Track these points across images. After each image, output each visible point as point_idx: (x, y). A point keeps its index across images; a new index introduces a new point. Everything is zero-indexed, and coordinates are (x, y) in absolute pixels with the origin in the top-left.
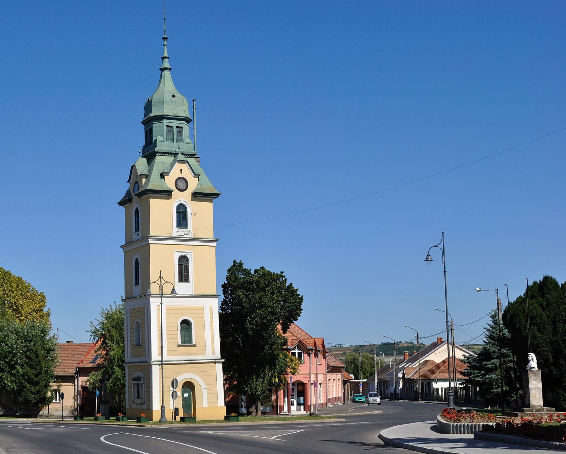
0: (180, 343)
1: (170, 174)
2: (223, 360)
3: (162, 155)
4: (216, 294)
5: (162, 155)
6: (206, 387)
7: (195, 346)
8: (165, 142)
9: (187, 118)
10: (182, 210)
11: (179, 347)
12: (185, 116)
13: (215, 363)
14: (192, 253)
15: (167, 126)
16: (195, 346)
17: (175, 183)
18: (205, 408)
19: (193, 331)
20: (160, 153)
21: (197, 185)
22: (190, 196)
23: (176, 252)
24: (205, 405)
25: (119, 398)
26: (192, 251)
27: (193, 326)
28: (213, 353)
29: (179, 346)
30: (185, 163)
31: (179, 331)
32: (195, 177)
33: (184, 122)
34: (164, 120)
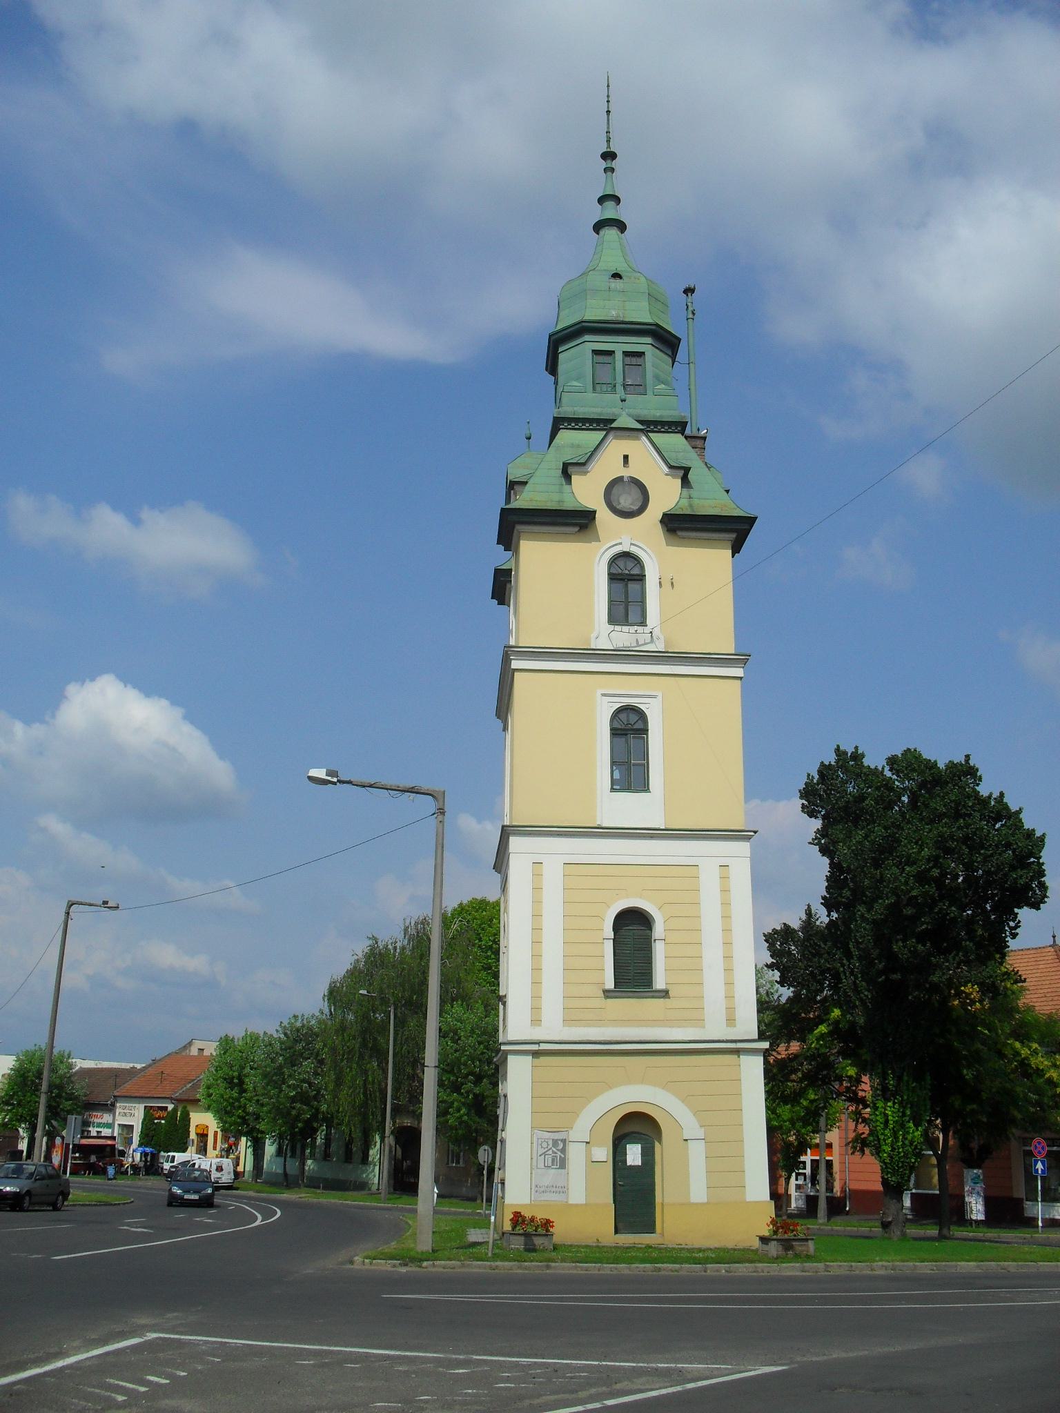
0: (610, 984)
1: (590, 467)
2: (766, 1045)
6: (700, 1133)
7: (665, 994)
8: (590, 395)
9: (657, 325)
10: (626, 567)
12: (650, 320)
13: (737, 1052)
14: (660, 698)
16: (665, 994)
19: (659, 951)
20: (570, 420)
23: (604, 695)
24: (698, 1192)
26: (660, 695)
27: (659, 930)
28: (731, 1021)
29: (607, 994)
31: (609, 948)
33: (649, 340)
34: (587, 337)
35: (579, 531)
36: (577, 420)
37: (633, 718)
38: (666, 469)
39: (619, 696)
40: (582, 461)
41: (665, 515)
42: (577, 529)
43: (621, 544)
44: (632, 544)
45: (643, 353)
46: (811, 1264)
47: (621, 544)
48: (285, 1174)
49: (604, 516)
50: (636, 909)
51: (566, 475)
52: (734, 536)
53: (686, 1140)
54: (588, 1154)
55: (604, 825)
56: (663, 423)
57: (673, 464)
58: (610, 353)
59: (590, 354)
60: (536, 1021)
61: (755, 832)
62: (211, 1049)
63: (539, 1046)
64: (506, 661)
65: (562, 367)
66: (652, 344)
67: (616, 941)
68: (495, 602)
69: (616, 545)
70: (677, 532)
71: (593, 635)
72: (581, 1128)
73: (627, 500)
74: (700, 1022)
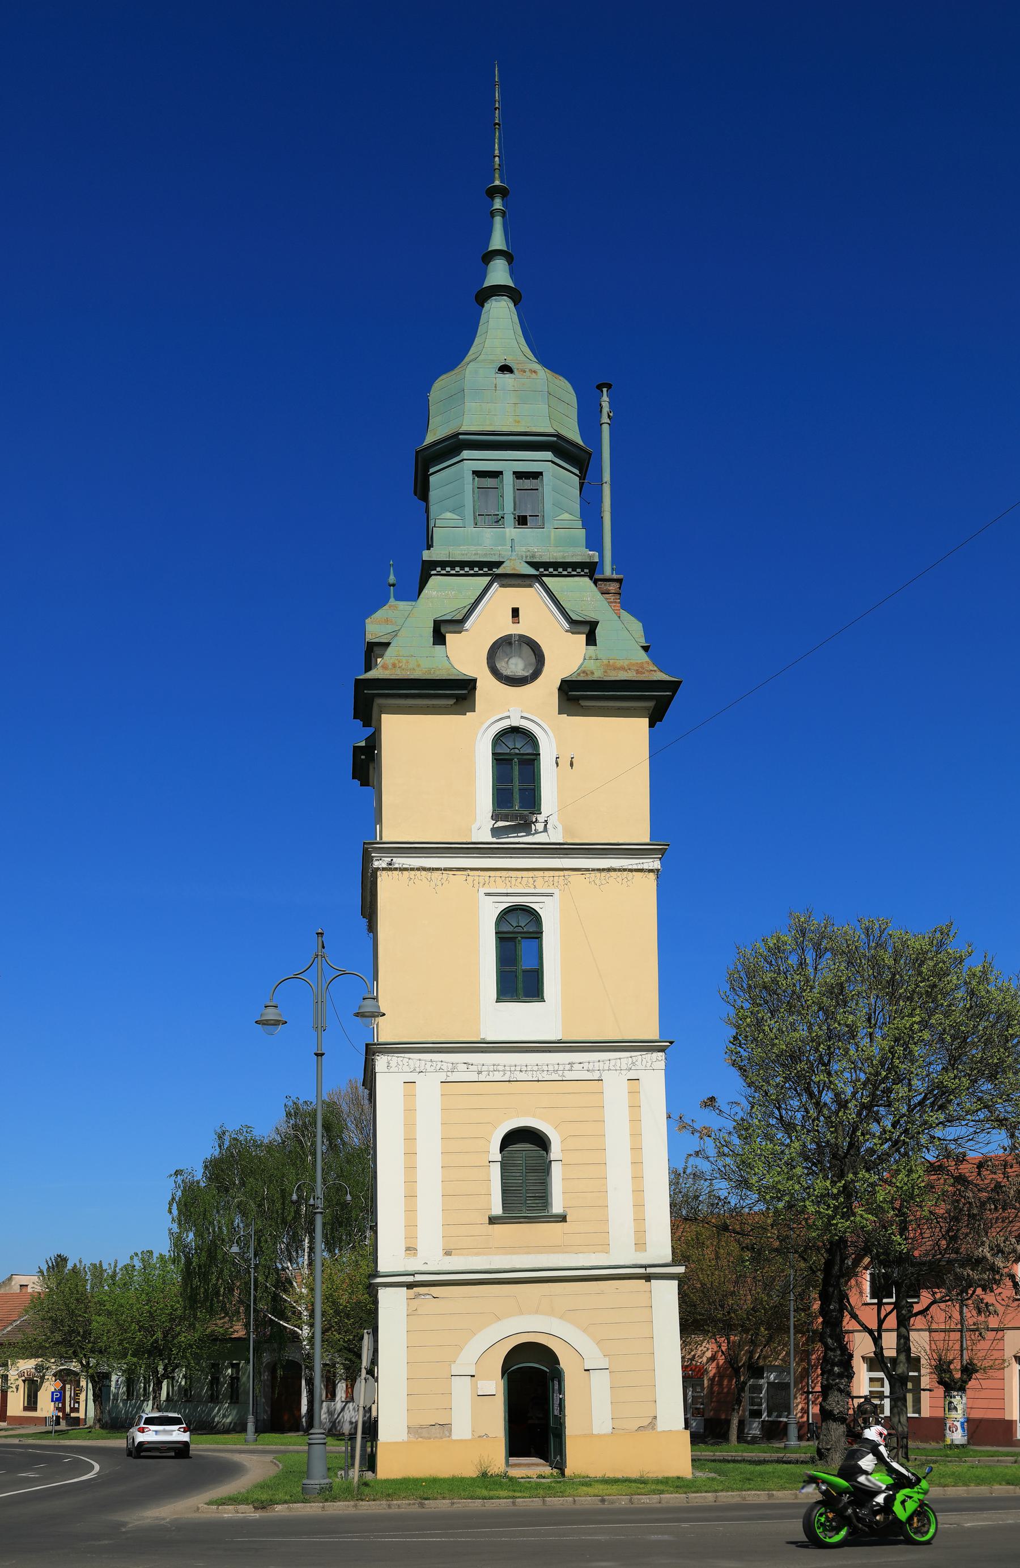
1: (467, 625)
2: (681, 1269)
4: (657, 1038)
5: (555, 573)
7: (563, 1218)
8: (471, 530)
9: (558, 436)
10: (519, 745)
11: (494, 1223)
12: (550, 430)
13: (648, 1278)
15: (478, 474)
16: (563, 1218)
17: (543, 664)
18: (599, 1436)
19: (556, 1170)
20: (443, 564)
21: (582, 660)
22: (554, 699)
23: (488, 894)
27: (556, 1151)
28: (640, 1245)
29: (493, 1220)
30: (531, 586)
31: (496, 1171)
32: (573, 633)
33: (549, 455)
34: (466, 454)
36: (453, 564)
37: (523, 920)
38: (566, 626)
39: (507, 895)
40: (459, 617)
41: (564, 682)
42: (451, 702)
43: (509, 717)
44: (522, 717)
45: (541, 473)
46: (725, 1493)
47: (509, 717)
49: (487, 685)
50: (528, 1129)
51: (439, 639)
52: (651, 704)
53: (588, 1370)
54: (474, 1387)
55: (489, 1039)
56: (565, 565)
57: (574, 617)
58: (497, 474)
59: (469, 476)
60: (411, 1250)
61: (671, 1043)
62: (34, 1284)
64: (367, 859)
65: (433, 494)
66: (553, 462)
67: (504, 1166)
68: (357, 782)
69: (501, 719)
70: (580, 702)
71: (474, 827)
72: (467, 1360)
73: (516, 666)
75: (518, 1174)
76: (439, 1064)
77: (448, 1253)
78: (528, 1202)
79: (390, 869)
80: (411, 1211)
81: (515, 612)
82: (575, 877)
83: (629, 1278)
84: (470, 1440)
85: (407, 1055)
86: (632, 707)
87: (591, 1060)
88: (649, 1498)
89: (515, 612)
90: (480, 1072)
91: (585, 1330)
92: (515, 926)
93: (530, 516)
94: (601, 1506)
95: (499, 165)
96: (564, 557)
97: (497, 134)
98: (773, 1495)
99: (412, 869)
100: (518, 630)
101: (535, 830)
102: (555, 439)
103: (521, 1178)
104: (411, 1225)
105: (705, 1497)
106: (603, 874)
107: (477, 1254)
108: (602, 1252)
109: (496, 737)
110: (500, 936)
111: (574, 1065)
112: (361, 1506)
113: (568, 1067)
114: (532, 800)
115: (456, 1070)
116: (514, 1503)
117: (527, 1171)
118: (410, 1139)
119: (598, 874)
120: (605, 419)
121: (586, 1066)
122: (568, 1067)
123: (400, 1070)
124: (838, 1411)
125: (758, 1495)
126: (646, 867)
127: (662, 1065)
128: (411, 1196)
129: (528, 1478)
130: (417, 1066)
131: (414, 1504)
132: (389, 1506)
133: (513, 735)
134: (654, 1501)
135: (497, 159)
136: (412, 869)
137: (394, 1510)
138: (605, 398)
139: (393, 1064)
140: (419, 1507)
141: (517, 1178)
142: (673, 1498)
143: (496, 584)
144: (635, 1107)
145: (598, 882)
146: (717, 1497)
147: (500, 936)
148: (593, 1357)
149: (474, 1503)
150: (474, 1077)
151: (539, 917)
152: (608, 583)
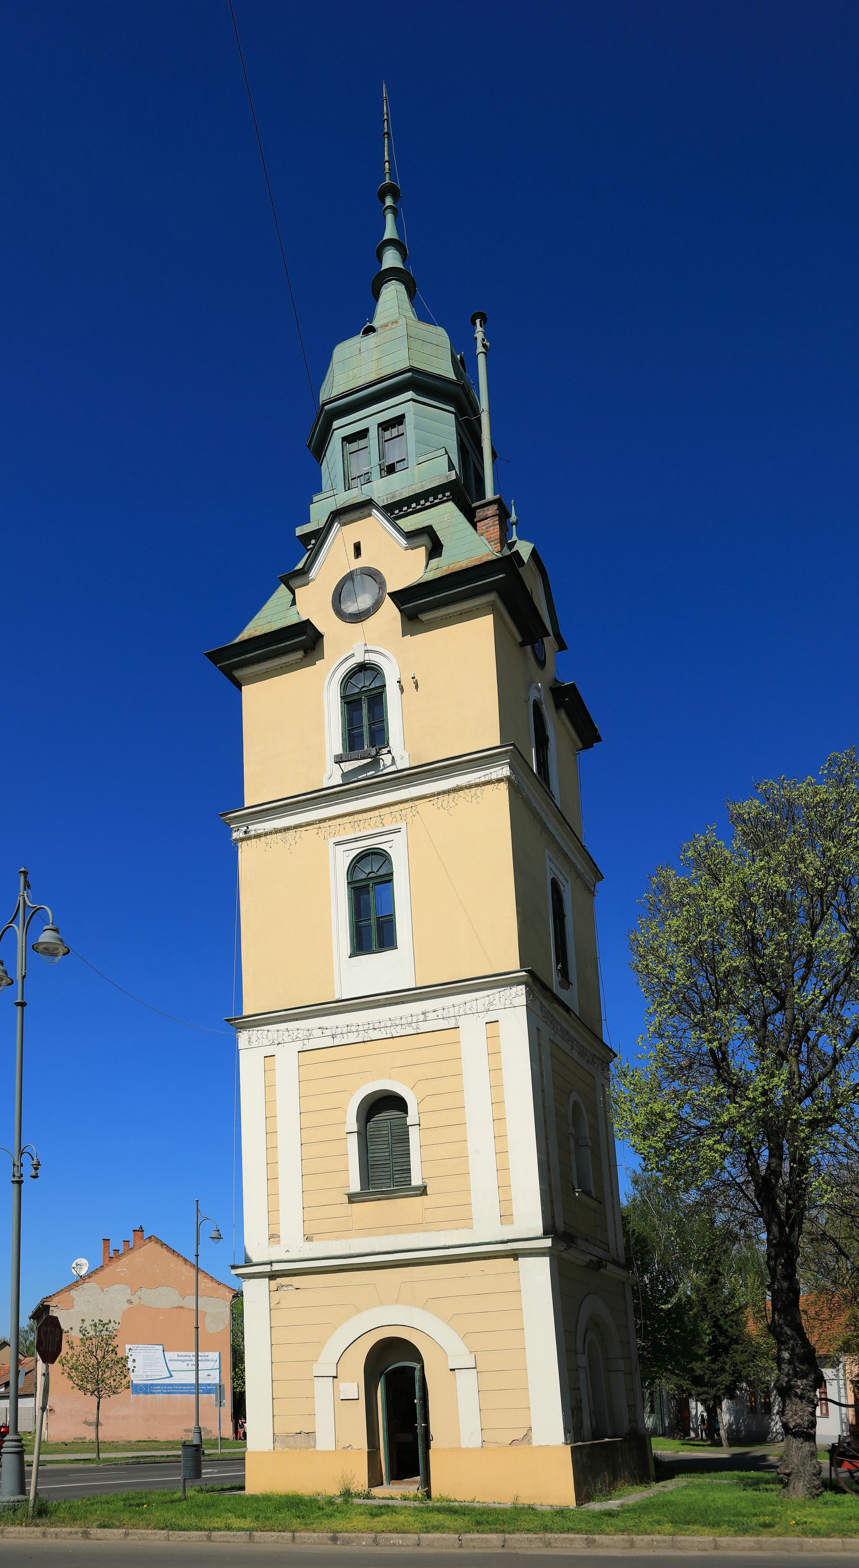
0: (355, 1186)
1: (312, 574)
3: (428, 504)
7: (423, 1191)
10: (363, 682)
11: (353, 1202)
13: (515, 1255)
16: (423, 1191)
18: (467, 1450)
23: (337, 844)
25: (669, 1370)
28: (506, 1217)
29: (352, 1198)
30: (370, 515)
31: (353, 1143)
32: (412, 549)
33: (410, 394)
34: (336, 424)
35: (304, 657)
38: (403, 542)
39: (356, 840)
42: (299, 654)
43: (353, 655)
44: (367, 651)
48: (197, 1384)
58: (363, 434)
60: (274, 1237)
63: (272, 1266)
69: (347, 659)
74: (467, 1222)
75: (385, 1146)
76: (296, 1032)
77: (308, 1238)
78: (396, 1176)
79: (249, 838)
80: (272, 1195)
81: (357, 548)
82: (422, 805)
83: (495, 1257)
84: (333, 1452)
85: (266, 1028)
86: (474, 607)
87: (445, 1005)
88: (402, 1538)
89: (357, 548)
90: (333, 1036)
91: (448, 1322)
92: (367, 872)
93: (397, 462)
94: (331, 1548)
95: (390, 170)
96: (423, 486)
97: (386, 142)
98: (594, 1541)
99: (266, 834)
100: (362, 562)
101: (384, 766)
102: (410, 374)
103: (388, 1150)
104: (273, 1211)
105: (487, 1541)
106: (452, 795)
107: (337, 1238)
108: (467, 1227)
109: (344, 682)
110: (353, 886)
111: (427, 1014)
112: (9, 1532)
113: (422, 1018)
114: (379, 737)
115: (311, 1037)
116: (209, 1538)
117: (393, 1142)
118: (270, 1117)
119: (446, 796)
120: (480, 349)
121: (440, 1013)
122: (422, 1018)
123: (261, 1045)
124: (794, 1424)
125: (571, 1540)
126: (494, 777)
127: (522, 1000)
128: (272, 1179)
129: (392, 1499)
130: (275, 1037)
131: (76, 1533)
132: (44, 1534)
133: (361, 675)
134: (410, 1542)
135: (387, 164)
136: (266, 834)
137: (50, 1541)
138: (479, 328)
139: (254, 1038)
140: (83, 1536)
141: (384, 1150)
142: (439, 1539)
143: (336, 524)
144: (494, 1054)
145: (445, 805)
146: (505, 1540)
147: (353, 886)
148: (458, 1355)
149: (155, 1534)
150: (329, 1042)
151: (387, 855)
152: (486, 508)
